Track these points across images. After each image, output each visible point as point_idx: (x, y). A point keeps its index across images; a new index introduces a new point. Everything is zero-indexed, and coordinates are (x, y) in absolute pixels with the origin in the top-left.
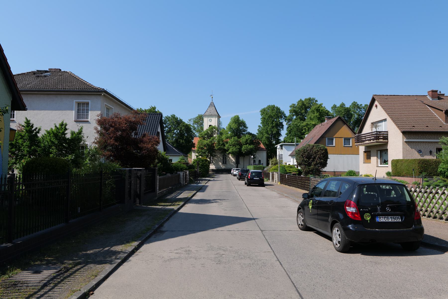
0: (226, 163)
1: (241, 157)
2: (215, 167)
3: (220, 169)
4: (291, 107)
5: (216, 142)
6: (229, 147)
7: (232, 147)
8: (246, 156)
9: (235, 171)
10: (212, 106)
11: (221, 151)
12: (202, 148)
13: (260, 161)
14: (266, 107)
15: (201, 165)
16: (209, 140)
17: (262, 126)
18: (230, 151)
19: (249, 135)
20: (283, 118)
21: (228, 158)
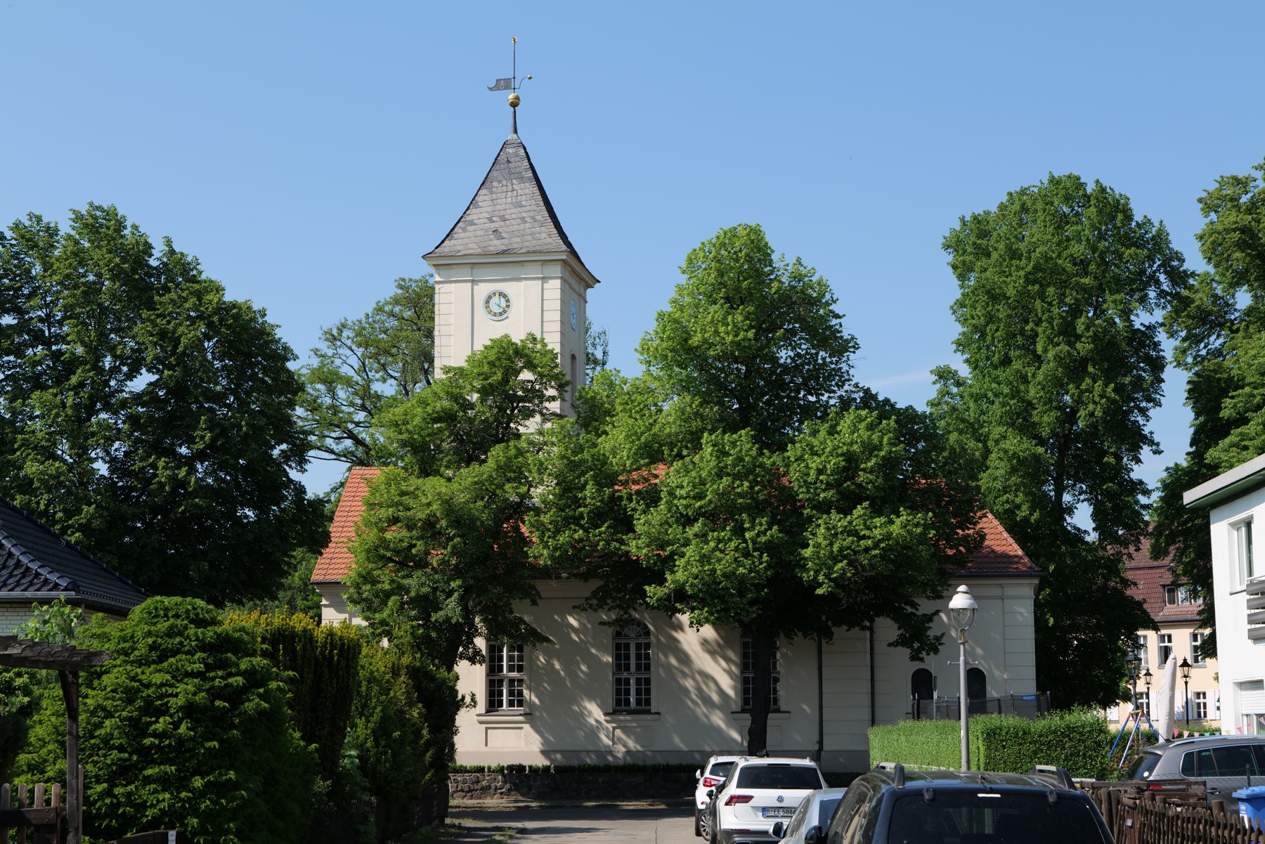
0: (644, 706)
1: (789, 636)
2: (545, 741)
3: (590, 760)
4: (1209, 205)
5: (539, 493)
6: (675, 531)
7: (703, 536)
8: (840, 632)
9: (733, 789)
10: (512, 175)
11: (595, 584)
12: (406, 560)
13: (976, 678)
14: (994, 209)
15: (189, 710)
16: (469, 475)
17: (964, 371)
18: (679, 575)
19: (869, 416)
20: (1162, 294)
21: (673, 661)
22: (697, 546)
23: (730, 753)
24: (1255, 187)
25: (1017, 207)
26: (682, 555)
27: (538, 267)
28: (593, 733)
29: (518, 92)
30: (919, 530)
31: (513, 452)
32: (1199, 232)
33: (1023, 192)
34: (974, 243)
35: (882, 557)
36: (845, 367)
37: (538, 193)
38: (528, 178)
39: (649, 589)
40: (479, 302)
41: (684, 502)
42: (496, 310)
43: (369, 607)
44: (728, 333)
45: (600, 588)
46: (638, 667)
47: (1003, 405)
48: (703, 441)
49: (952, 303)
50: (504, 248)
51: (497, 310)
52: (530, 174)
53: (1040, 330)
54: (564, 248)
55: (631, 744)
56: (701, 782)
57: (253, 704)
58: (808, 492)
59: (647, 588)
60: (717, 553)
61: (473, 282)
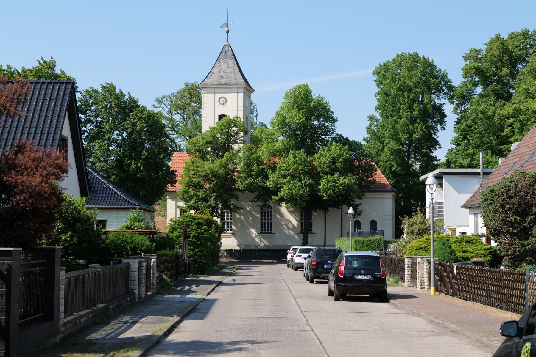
0: (270, 231)
2: (239, 242)
3: (253, 248)
4: (466, 58)
5: (239, 168)
7: (289, 181)
9: (297, 254)
10: (227, 57)
11: (256, 194)
12: (198, 186)
16: (218, 161)
17: (379, 117)
18: (283, 193)
21: (278, 216)
22: (288, 184)
23: (297, 246)
24: (482, 53)
25: (399, 60)
26: (283, 187)
27: (236, 89)
28: (253, 239)
29: (229, 28)
30: (354, 181)
31: (232, 154)
32: (463, 67)
33: (402, 54)
34: (383, 74)
35: (343, 189)
36: (333, 127)
37: (235, 63)
38: (232, 58)
39: (273, 197)
40: (217, 100)
41: (284, 172)
42: (222, 103)
43: (186, 201)
44: (297, 120)
45: (257, 196)
46: (268, 219)
47: (389, 131)
48: (290, 153)
49: (375, 93)
50: (225, 82)
51: (222, 103)
52: (233, 57)
53: (401, 107)
54: (245, 83)
55: (266, 243)
56: (289, 253)
57: (206, 235)
58: (321, 169)
59: (273, 197)
60: (293, 187)
61: (215, 93)
